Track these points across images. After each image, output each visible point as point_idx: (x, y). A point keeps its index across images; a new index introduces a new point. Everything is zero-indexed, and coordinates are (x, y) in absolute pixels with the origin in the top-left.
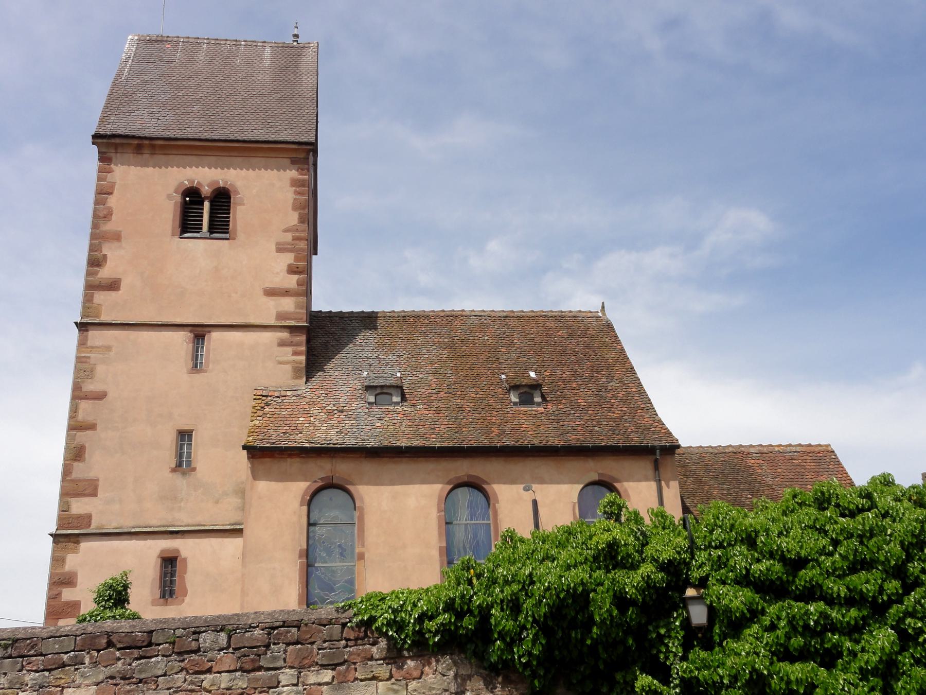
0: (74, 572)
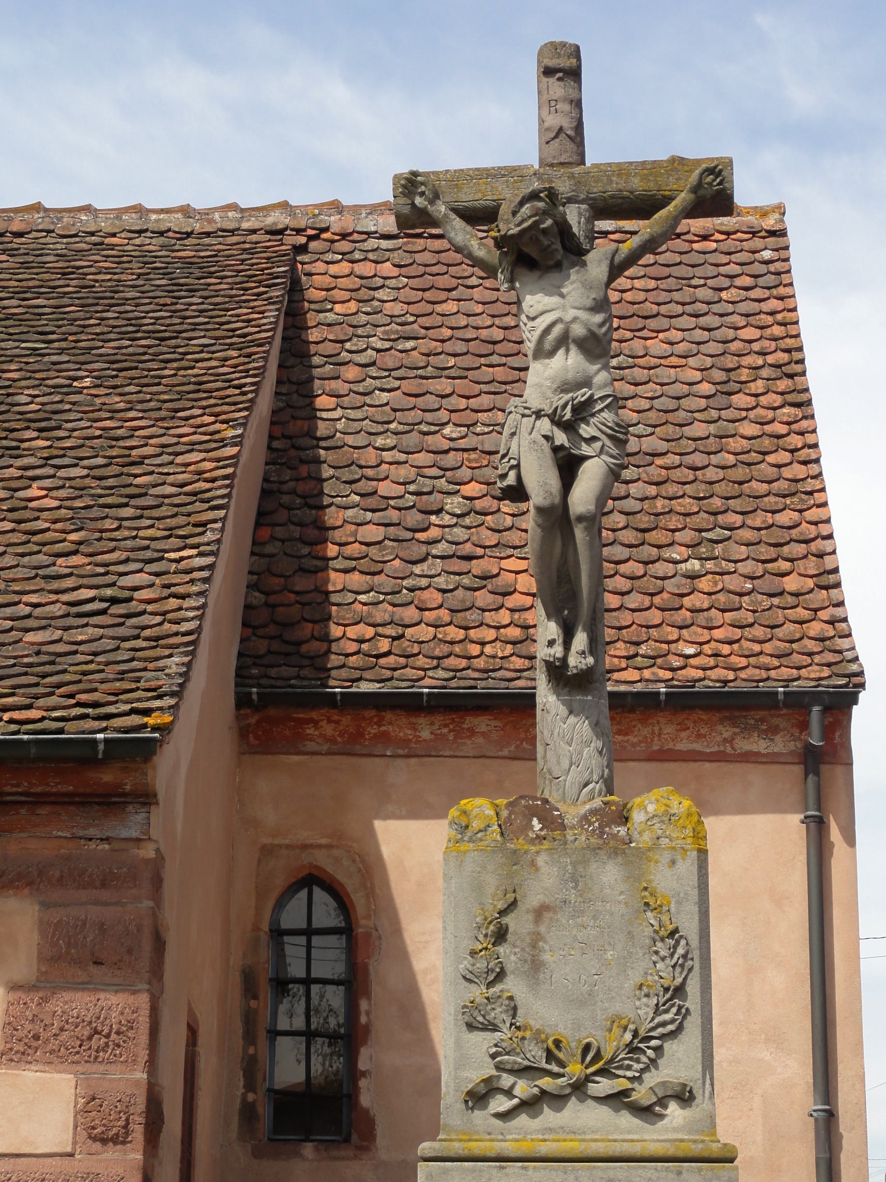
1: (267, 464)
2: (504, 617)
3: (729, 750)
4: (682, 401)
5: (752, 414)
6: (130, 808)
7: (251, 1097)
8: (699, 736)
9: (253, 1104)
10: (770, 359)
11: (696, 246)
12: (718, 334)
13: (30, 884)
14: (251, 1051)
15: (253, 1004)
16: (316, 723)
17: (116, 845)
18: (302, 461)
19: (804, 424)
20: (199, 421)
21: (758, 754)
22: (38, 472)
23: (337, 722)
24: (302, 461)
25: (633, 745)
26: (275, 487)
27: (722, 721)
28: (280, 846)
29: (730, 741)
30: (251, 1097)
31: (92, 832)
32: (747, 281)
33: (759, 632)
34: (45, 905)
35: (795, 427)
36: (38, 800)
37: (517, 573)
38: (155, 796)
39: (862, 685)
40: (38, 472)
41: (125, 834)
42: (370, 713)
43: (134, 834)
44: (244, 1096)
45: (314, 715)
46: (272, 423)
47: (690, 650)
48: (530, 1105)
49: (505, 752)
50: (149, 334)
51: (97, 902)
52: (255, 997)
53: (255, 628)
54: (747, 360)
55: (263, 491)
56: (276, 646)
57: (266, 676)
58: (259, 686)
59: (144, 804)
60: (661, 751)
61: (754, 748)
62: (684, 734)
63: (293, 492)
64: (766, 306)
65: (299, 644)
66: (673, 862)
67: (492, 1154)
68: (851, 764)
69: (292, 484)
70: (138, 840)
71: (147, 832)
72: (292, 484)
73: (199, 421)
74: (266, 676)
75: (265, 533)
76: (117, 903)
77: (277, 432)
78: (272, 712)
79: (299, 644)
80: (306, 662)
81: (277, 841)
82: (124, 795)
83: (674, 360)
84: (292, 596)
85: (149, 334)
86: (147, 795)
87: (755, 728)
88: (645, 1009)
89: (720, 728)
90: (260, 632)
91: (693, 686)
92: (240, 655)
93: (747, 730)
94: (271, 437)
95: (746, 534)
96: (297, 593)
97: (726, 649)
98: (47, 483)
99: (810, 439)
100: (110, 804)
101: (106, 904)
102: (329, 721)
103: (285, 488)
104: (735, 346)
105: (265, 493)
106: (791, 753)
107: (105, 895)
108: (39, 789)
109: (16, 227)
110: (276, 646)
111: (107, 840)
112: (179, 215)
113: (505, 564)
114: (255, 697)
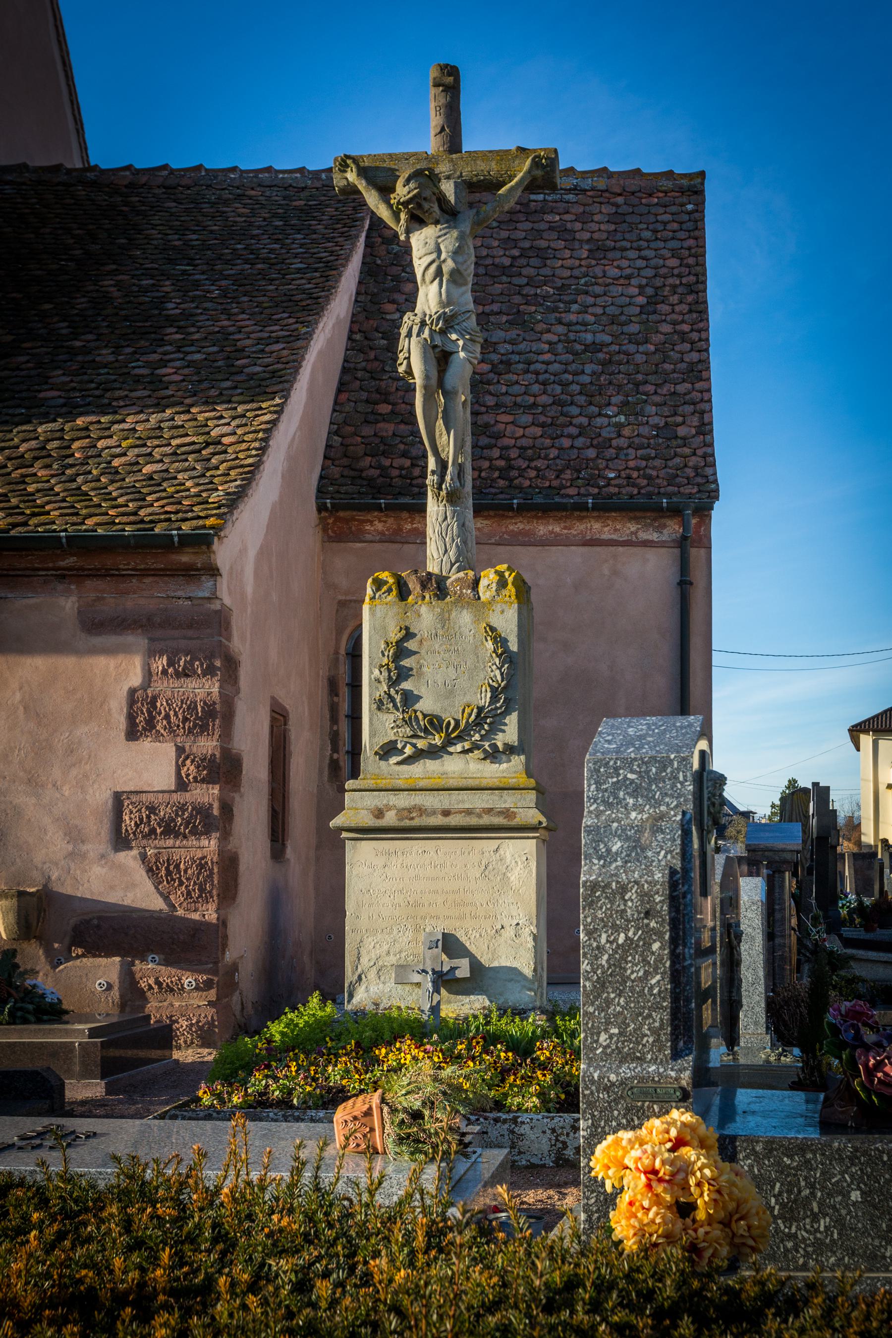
0: (331, 540)
1: (347, 350)
2: (496, 453)
3: (634, 539)
4: (625, 309)
5: (669, 318)
6: (203, 578)
7: (335, 756)
8: (616, 530)
9: (337, 761)
10: (684, 281)
11: (644, 201)
12: (653, 263)
13: (141, 626)
14: (335, 728)
15: (335, 699)
16: (371, 522)
17: (196, 602)
18: (371, 348)
19: (701, 325)
20: (285, 322)
21: (652, 541)
22: (172, 356)
23: (385, 522)
24: (371, 348)
25: (574, 536)
26: (352, 365)
27: (631, 519)
28: (351, 601)
29: (635, 533)
30: (335, 756)
31: (179, 593)
32: (675, 226)
33: (658, 463)
34: (152, 640)
35: (695, 327)
36: (145, 573)
37: (507, 424)
38: (218, 570)
39: (717, 498)
40: (172, 356)
41: (201, 594)
42: (405, 515)
43: (207, 595)
44: (331, 757)
45: (369, 517)
46: (352, 322)
47: (612, 475)
48: (419, 755)
49: (493, 541)
50: (265, 261)
51: (185, 638)
52: (337, 695)
53: (333, 460)
54: (670, 281)
55: (344, 368)
56: (346, 472)
57: (338, 492)
58: (332, 498)
59: (213, 575)
60: (591, 539)
61: (650, 538)
62: (606, 529)
63: (365, 369)
64: (686, 244)
65: (362, 471)
66: (503, 612)
67: (390, 787)
68: (709, 548)
69: (364, 364)
70: (209, 598)
71: (215, 593)
72: (364, 364)
73: (285, 322)
74: (338, 492)
75: (343, 397)
76: (198, 638)
77: (356, 329)
78: (341, 514)
79: (362, 471)
80: (365, 483)
81: (348, 598)
82: (198, 570)
83: (622, 281)
84: (359, 439)
85: (265, 261)
86: (213, 569)
87: (651, 525)
88: (484, 699)
89: (629, 525)
90: (337, 462)
91: (83, 523)
92: (321, 477)
93: (646, 527)
94: (351, 331)
95: (657, 399)
96: (363, 437)
97: (635, 474)
98: (178, 364)
99: (703, 335)
100: (190, 576)
101: (190, 639)
102: (380, 521)
103: (359, 366)
104: (663, 271)
105: (345, 370)
106: (673, 541)
107: (190, 633)
108: (142, 567)
109: (185, 182)
110: (346, 472)
111: (189, 598)
112: (298, 175)
113: (499, 418)
114: (329, 505)
